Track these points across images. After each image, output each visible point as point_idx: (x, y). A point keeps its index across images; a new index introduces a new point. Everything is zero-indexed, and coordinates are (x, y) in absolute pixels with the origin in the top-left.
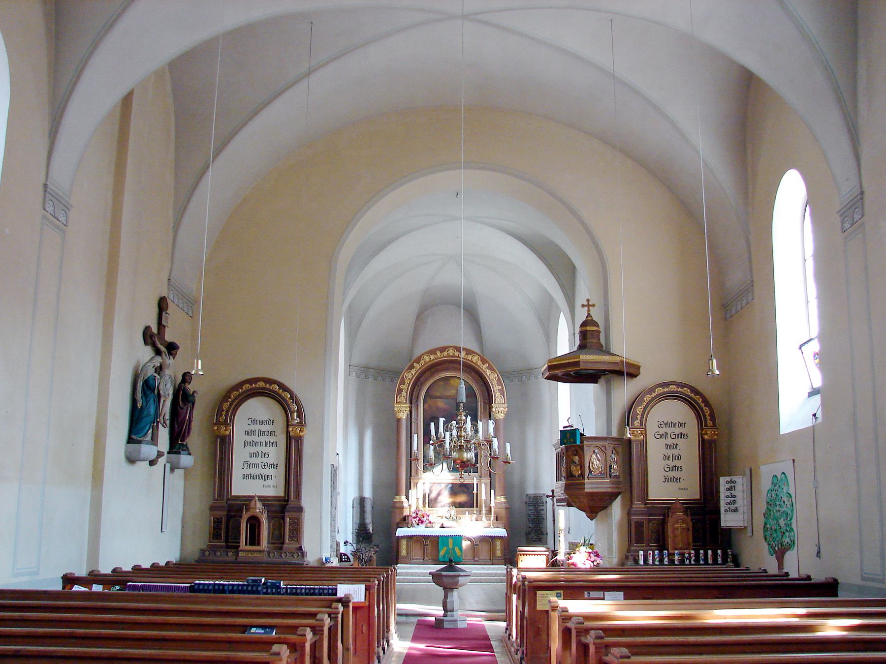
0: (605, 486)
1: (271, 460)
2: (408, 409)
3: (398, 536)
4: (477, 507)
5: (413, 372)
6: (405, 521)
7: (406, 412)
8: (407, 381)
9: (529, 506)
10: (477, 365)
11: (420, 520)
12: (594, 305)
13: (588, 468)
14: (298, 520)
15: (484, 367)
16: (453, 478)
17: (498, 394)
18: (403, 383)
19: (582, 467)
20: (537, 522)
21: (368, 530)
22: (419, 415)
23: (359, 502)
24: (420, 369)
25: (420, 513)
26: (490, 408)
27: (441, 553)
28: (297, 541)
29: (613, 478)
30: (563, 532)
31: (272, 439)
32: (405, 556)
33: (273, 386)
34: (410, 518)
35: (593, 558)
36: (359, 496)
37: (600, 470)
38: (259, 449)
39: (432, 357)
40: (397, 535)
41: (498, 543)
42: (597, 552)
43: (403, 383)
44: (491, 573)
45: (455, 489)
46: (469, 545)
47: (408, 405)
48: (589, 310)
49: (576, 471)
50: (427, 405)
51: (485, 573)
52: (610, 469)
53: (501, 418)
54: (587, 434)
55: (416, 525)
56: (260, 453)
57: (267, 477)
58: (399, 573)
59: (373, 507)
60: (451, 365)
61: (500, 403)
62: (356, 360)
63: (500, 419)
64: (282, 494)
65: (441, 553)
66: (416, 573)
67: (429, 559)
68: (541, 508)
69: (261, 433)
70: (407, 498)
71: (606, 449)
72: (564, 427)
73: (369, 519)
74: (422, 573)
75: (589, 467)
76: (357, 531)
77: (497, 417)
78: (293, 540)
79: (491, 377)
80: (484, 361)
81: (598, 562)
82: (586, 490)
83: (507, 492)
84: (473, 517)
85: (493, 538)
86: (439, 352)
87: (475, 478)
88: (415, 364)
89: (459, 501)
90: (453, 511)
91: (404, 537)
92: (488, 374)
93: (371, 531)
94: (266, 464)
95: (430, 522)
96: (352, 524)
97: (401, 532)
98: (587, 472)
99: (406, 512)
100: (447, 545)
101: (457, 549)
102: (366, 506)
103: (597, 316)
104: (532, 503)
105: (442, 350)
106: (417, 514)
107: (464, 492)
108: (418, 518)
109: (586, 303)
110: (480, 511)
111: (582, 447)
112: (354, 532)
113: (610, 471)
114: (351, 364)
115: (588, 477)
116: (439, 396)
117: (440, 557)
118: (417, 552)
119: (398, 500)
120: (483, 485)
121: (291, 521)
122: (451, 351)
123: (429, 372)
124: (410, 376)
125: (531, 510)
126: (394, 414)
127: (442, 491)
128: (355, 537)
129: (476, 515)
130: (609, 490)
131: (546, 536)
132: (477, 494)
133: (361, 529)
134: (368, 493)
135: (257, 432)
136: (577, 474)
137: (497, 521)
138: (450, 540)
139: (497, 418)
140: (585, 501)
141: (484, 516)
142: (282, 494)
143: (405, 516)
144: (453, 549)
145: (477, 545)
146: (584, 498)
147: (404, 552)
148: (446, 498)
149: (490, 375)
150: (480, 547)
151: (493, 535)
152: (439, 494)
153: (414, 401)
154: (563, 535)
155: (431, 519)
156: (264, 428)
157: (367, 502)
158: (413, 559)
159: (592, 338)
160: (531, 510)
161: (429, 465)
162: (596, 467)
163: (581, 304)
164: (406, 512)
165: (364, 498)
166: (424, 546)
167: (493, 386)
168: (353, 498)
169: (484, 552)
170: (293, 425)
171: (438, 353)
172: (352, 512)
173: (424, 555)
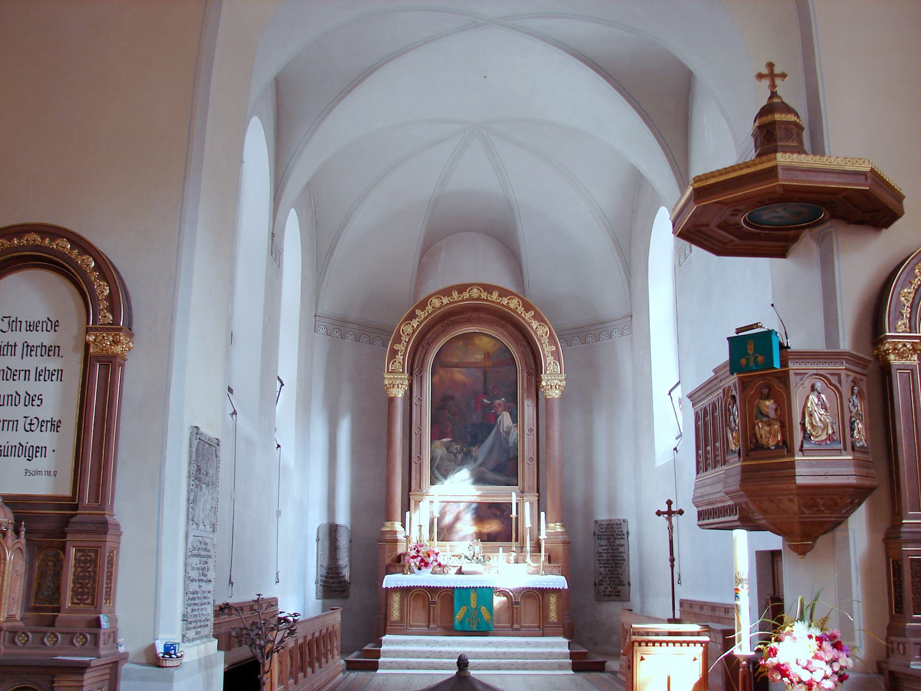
0: (844, 470)
1: (46, 412)
2: (406, 382)
3: (387, 588)
4: (517, 540)
5: (415, 323)
6: (398, 563)
7: (404, 386)
8: (405, 338)
9: (601, 539)
10: (517, 313)
11: (422, 560)
12: (783, 76)
13: (799, 427)
14: (97, 552)
15: (528, 316)
16: (479, 493)
17: (550, 359)
18: (398, 340)
19: (784, 421)
20: (613, 565)
21: (343, 577)
22: (424, 393)
23: (328, 532)
24: (426, 318)
25: (423, 550)
26: (538, 381)
27: (458, 616)
28: (92, 604)
29: (859, 452)
30: (746, 586)
31: (52, 364)
32: (395, 622)
33: (84, 257)
34: (407, 558)
35: (830, 652)
36: (328, 523)
37: (830, 432)
38: (22, 386)
39: (445, 300)
40: (384, 586)
41: (553, 600)
42: (835, 637)
43: (398, 340)
44: (543, 653)
45: (483, 512)
46: (504, 602)
47: (406, 375)
48: (773, 86)
49: (769, 435)
50: (436, 378)
51: (531, 653)
52: (852, 430)
53: (556, 397)
54: (795, 344)
55: (416, 570)
56: (23, 395)
57: (36, 451)
58: (385, 652)
59: (350, 541)
60: (475, 315)
61: (554, 373)
62: (326, 307)
63: (554, 398)
64: (67, 491)
65: (457, 617)
66: (414, 651)
67: (438, 627)
68: (618, 542)
69: (29, 349)
70: (404, 526)
71: (840, 382)
72: (739, 330)
73: (344, 560)
74: (424, 652)
75: (803, 425)
76: (324, 579)
77: (550, 395)
78: (82, 601)
79: (540, 332)
80: (528, 307)
81: (843, 664)
82: (800, 481)
83: (565, 516)
84: (510, 557)
85: (544, 592)
86: (456, 293)
87: (514, 494)
88: (418, 312)
89: (489, 530)
90: (478, 547)
91: (396, 589)
92: (535, 327)
93: (347, 578)
94: (35, 421)
95: (440, 565)
96: (315, 569)
97: (391, 581)
98: (798, 436)
99: (401, 549)
100: (467, 603)
101: (483, 609)
102: (338, 538)
103: (789, 93)
104: (605, 535)
105: (462, 288)
106: (418, 551)
107: (495, 517)
108: (419, 558)
109: (765, 71)
110: (522, 548)
111: (783, 378)
112: (319, 581)
113: (852, 436)
114: (317, 315)
115: (801, 450)
116: (457, 364)
117: (456, 623)
118: (418, 616)
119: (388, 529)
120: (527, 505)
121: (79, 554)
122: (475, 290)
123: (439, 326)
124: (410, 330)
125: (601, 546)
126: (383, 389)
127: (462, 514)
128: (321, 588)
129: (515, 554)
130: (853, 480)
131: (628, 587)
132: (517, 519)
133: (331, 575)
134: (343, 518)
135: (19, 349)
136: (772, 443)
137: (549, 562)
138: (473, 595)
139: (549, 397)
140: (794, 507)
141: (528, 555)
142: (67, 491)
143: (400, 555)
144: (477, 609)
145: (517, 603)
146: (791, 500)
147: (395, 614)
148: (467, 527)
149: (537, 328)
150: (522, 606)
151: (544, 587)
152: (457, 519)
153: (416, 370)
154: (747, 591)
155: (440, 559)
156: (37, 338)
157: (341, 533)
158: (410, 626)
159: (788, 139)
160: (601, 546)
161: (440, 472)
162: (820, 424)
163: (756, 73)
164: (401, 549)
165: (337, 526)
166: (429, 604)
167: (542, 347)
168: (318, 526)
169: (529, 614)
170: (96, 329)
171: (455, 295)
172: (316, 548)
173: (429, 618)
